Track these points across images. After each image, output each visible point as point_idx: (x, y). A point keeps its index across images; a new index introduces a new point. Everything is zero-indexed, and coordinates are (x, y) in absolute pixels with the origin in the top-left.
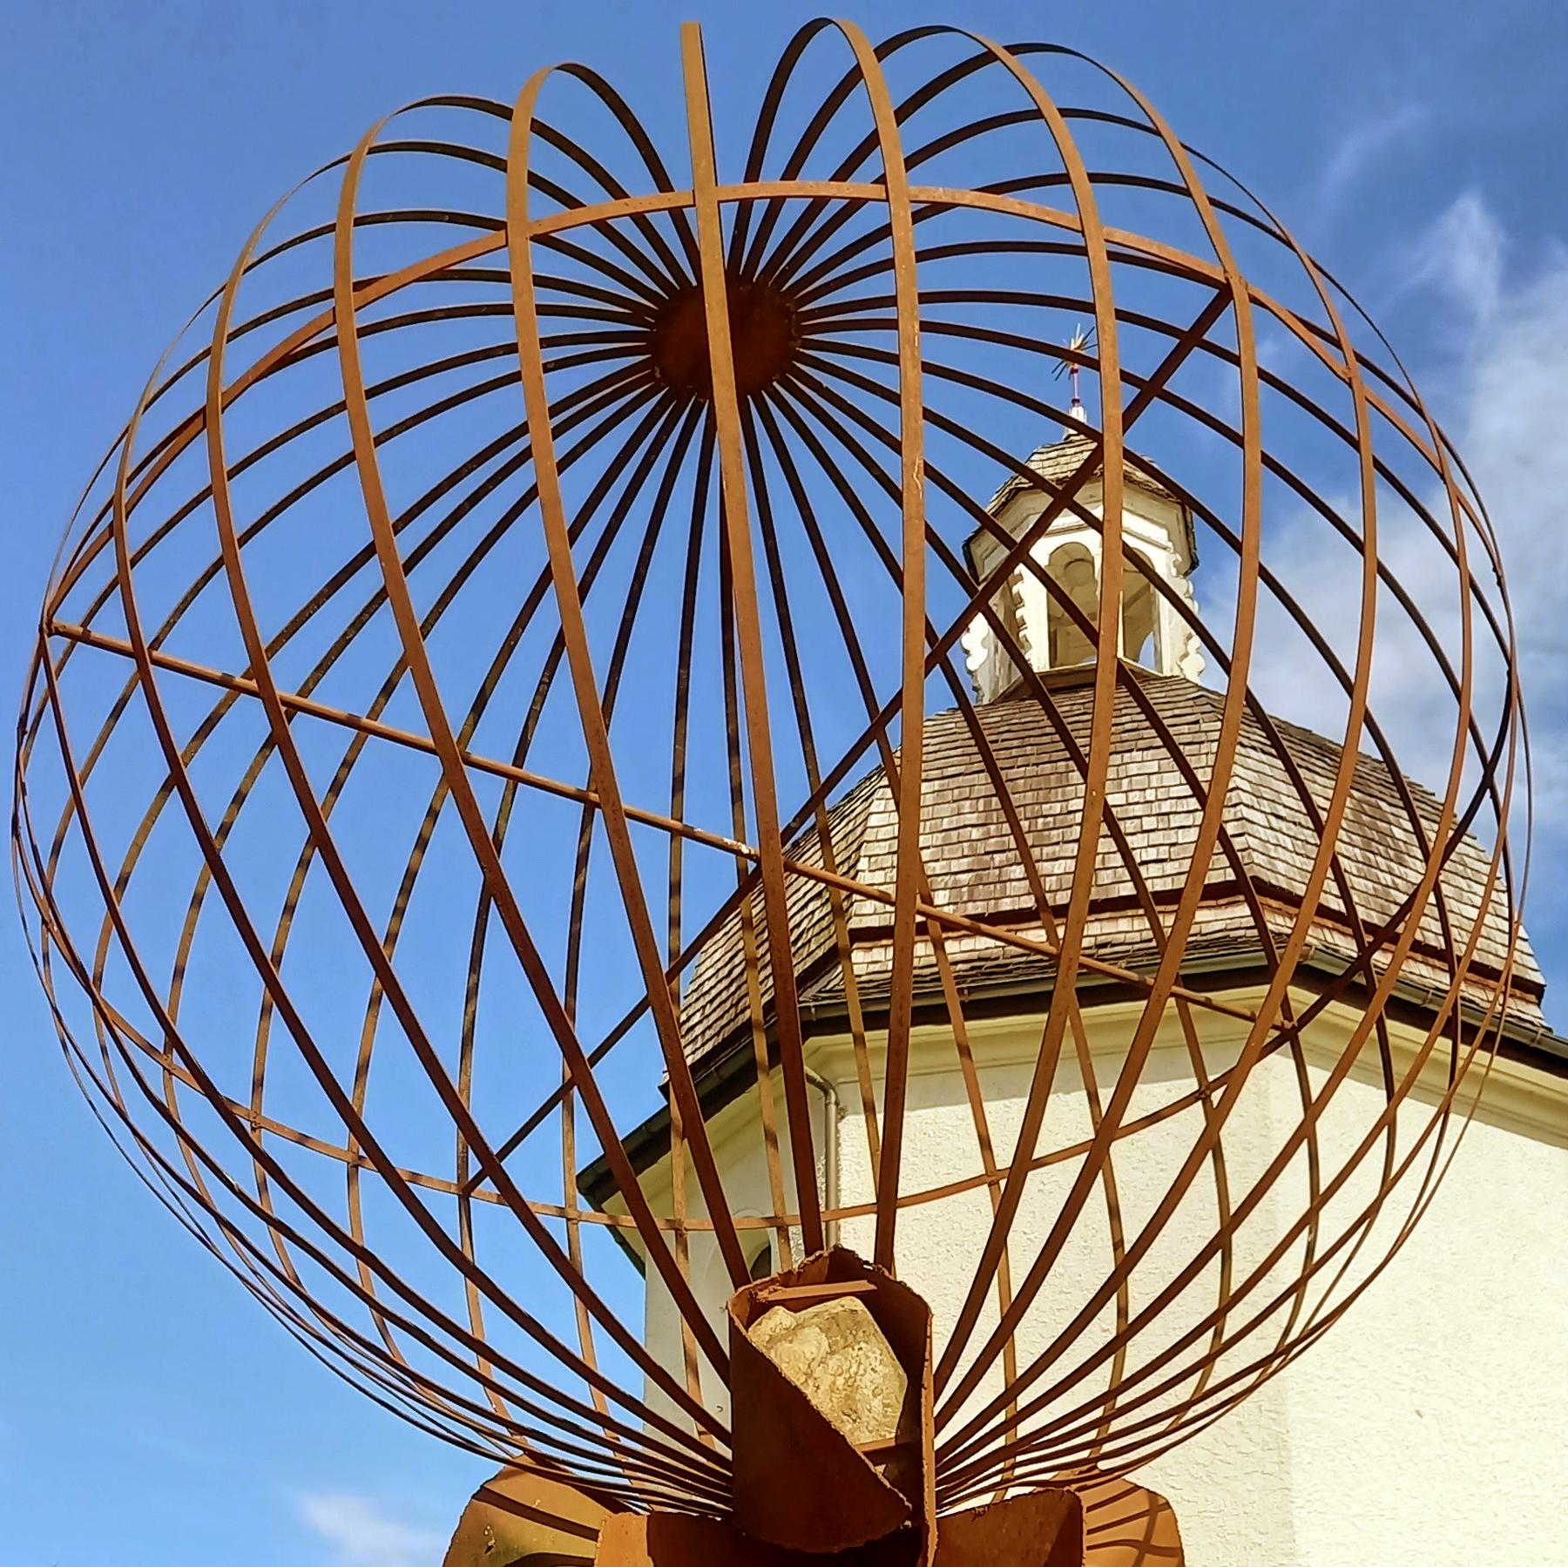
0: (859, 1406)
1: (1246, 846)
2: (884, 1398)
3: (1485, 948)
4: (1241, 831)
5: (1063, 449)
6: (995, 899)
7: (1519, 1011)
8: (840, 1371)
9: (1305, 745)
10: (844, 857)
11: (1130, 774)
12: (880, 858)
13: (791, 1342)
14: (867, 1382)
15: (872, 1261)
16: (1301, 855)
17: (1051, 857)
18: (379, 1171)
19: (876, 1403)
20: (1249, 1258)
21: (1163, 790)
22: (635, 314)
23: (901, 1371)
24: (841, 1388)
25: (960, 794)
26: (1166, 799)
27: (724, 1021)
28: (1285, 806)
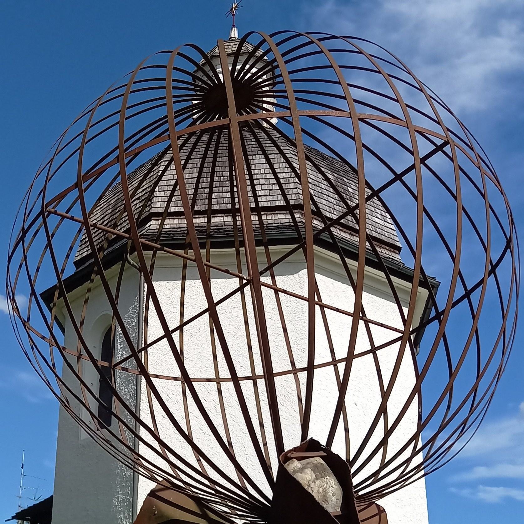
0: (328, 499)
1: (297, 192)
2: (336, 497)
3: (381, 233)
4: (295, 187)
5: (230, 43)
6: (204, 205)
7: (392, 256)
8: (320, 486)
9: (317, 156)
10: (149, 185)
11: (255, 163)
12: (163, 187)
13: (301, 473)
14: (330, 491)
15: (325, 446)
16: (317, 197)
17: (226, 191)
18: (91, 361)
19: (334, 498)
20: (296, 343)
21: (267, 170)
22: (202, 89)
23: (340, 487)
24: (321, 492)
25: (193, 166)
26: (268, 173)
27: (100, 241)
28: (311, 179)
